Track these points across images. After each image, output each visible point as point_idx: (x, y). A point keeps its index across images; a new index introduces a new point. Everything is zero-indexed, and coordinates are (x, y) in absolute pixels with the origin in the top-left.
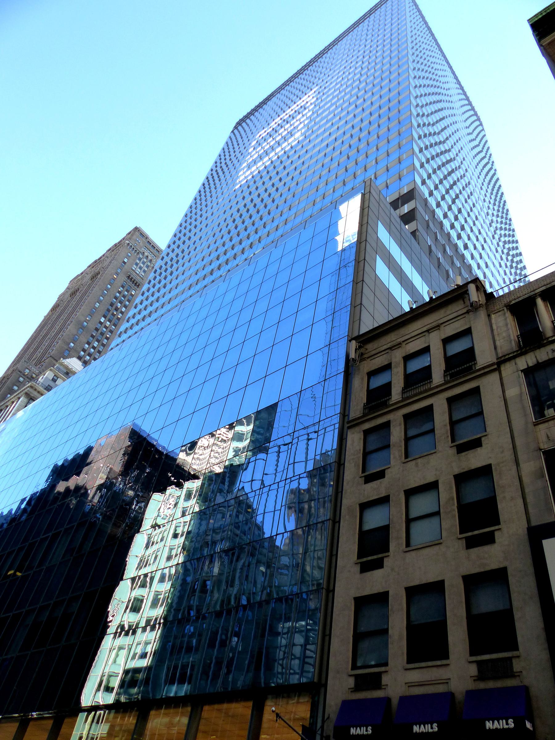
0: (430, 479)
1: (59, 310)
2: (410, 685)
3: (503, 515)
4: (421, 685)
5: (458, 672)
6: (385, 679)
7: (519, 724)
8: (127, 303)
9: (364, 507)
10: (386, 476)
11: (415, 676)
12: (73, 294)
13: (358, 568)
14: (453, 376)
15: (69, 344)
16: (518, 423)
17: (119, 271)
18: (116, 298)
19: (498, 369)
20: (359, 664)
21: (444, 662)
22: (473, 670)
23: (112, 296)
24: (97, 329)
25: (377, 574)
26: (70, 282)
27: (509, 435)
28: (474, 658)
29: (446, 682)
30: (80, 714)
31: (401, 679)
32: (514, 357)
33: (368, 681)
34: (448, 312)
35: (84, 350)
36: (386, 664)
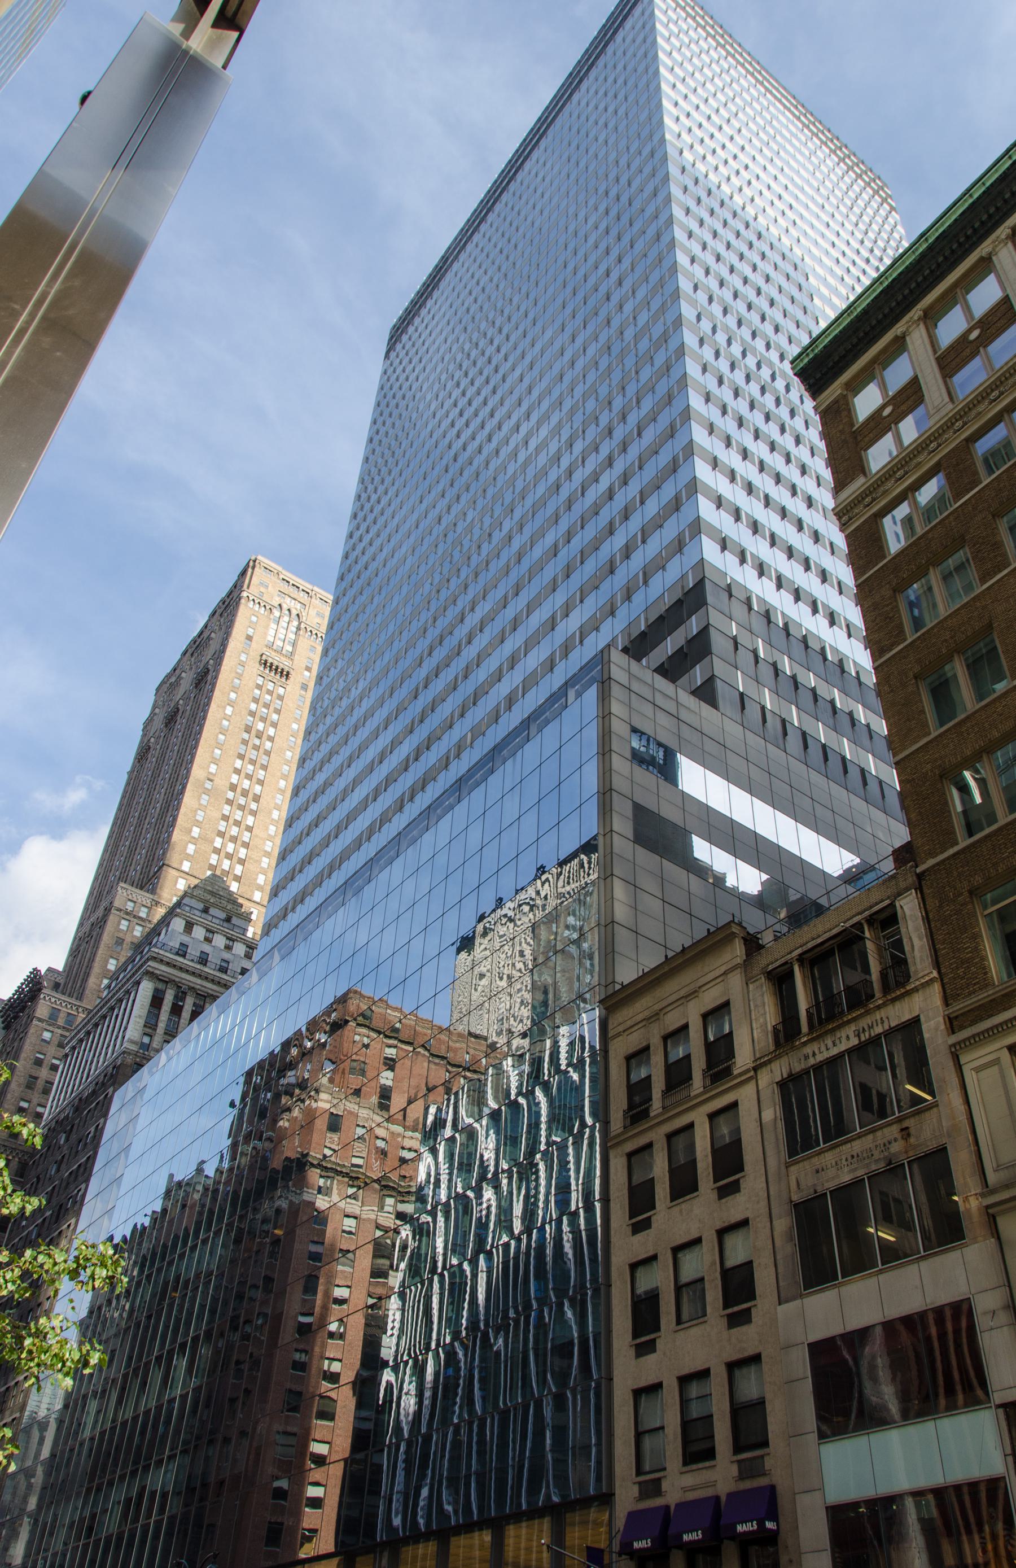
0: (694, 1235)
1: (152, 758)
2: (685, 1490)
3: (759, 1289)
4: (693, 1489)
5: (721, 1476)
6: (665, 1485)
7: (761, 1524)
8: (275, 717)
9: (634, 1267)
10: (653, 1225)
11: (689, 1480)
12: (170, 720)
13: (632, 1352)
14: (713, 1082)
15: (191, 831)
16: (772, 1162)
17: (243, 657)
18: (252, 714)
19: (755, 1077)
20: (647, 1468)
21: (712, 1463)
22: (734, 1470)
23: (245, 712)
24: (233, 788)
25: (651, 1358)
26: (158, 690)
27: (763, 1179)
28: (735, 1458)
29: (714, 1484)
30: (696, 855)
31: (680, 1484)
32: (770, 1061)
33: (651, 1488)
34: (706, 970)
35: (221, 834)
36: (665, 1469)
